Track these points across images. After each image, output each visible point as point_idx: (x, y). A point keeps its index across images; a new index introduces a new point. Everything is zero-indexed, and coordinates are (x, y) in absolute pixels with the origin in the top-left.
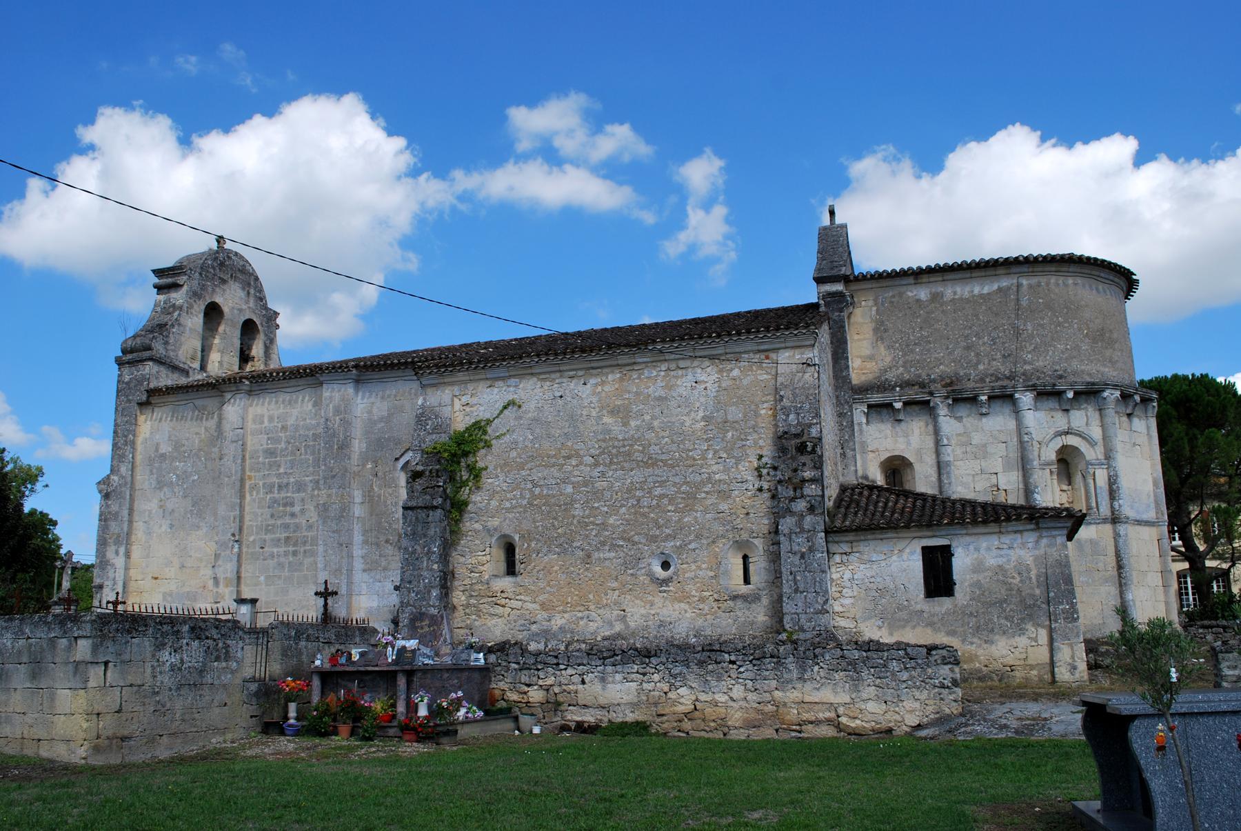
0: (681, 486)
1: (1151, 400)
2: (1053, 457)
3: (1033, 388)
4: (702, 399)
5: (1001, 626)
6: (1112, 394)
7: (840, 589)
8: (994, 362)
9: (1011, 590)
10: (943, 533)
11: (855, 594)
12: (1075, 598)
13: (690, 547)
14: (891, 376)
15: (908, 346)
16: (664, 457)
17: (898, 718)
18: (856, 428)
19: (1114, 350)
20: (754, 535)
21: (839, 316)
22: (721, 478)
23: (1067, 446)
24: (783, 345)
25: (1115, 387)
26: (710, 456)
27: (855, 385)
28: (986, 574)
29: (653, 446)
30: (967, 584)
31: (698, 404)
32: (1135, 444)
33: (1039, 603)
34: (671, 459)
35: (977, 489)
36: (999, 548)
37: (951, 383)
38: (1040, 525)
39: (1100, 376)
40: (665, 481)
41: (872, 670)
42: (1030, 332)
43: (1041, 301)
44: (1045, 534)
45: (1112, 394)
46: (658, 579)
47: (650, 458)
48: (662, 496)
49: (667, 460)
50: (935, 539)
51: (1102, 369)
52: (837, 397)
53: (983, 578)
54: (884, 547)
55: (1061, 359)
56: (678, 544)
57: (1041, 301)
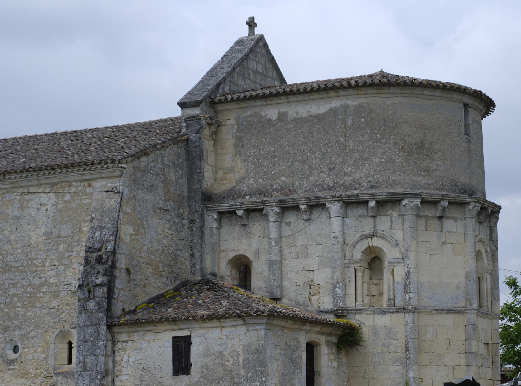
0: (27, 288)
4: (44, 219)
7: (120, 368)
8: (322, 174)
9: (226, 370)
10: (185, 327)
11: (129, 372)
13: (30, 335)
15: (258, 160)
16: (16, 264)
20: (73, 326)
22: (54, 281)
23: (373, 247)
24: (99, 176)
25: (414, 196)
26: (48, 264)
28: (211, 358)
29: (10, 256)
30: (199, 366)
31: (41, 223)
32: (444, 243)
33: (242, 380)
34: (20, 266)
35: (298, 284)
36: (220, 339)
40: (17, 284)
42: (351, 147)
43: (363, 120)
44: (251, 328)
45: (412, 202)
46: (8, 360)
47: (7, 265)
48: (13, 296)
49: (18, 267)
50: (181, 331)
53: (209, 361)
54: (149, 336)
56: (23, 333)
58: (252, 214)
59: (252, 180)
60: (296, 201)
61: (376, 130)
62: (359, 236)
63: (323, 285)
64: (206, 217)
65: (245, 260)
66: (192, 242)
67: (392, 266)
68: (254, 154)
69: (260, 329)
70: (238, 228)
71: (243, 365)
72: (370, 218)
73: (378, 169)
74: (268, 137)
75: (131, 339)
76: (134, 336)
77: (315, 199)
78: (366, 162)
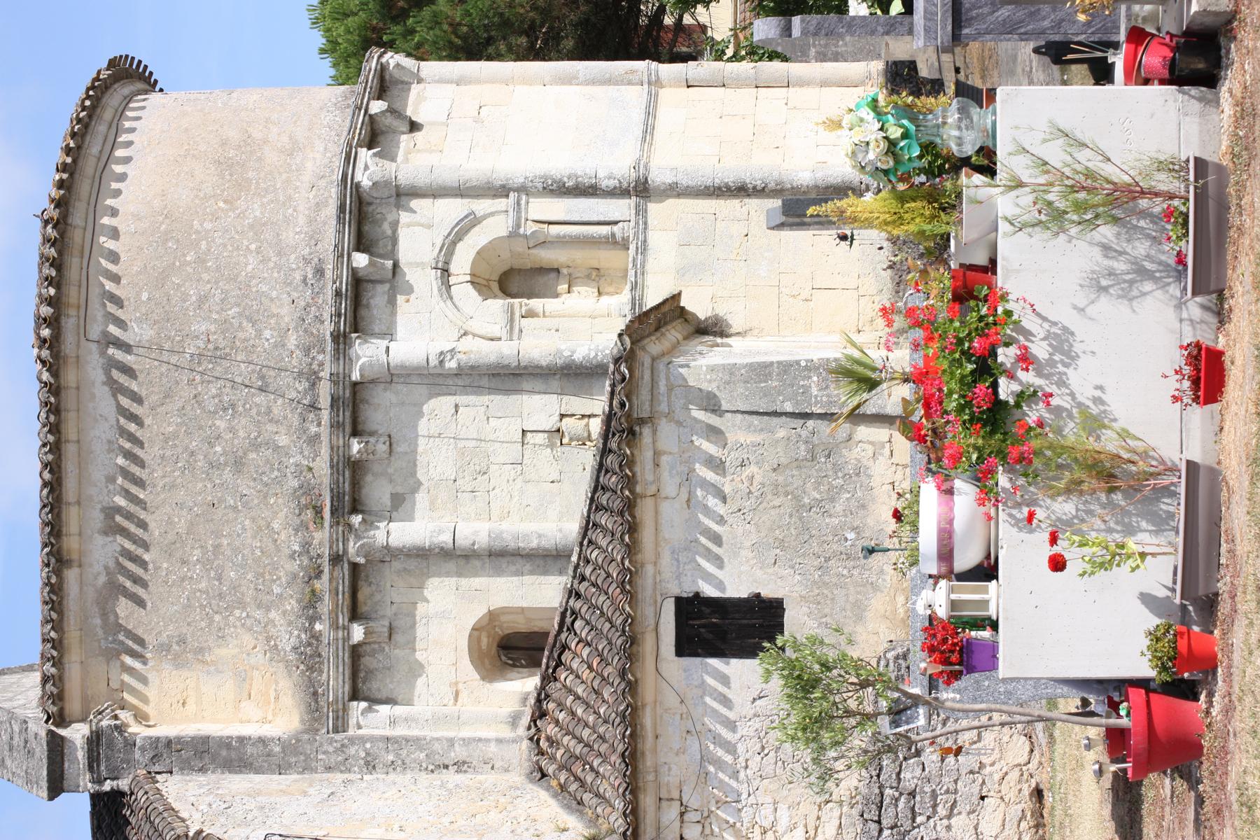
1: (383, 69)
2: (498, 305)
3: (341, 341)
5: (848, 512)
6: (366, 168)
7: (757, 830)
8: (276, 411)
12: (798, 363)
14: (288, 639)
17: (1015, 774)
18: (399, 731)
19: (266, 141)
21: (143, 749)
23: (472, 275)
27: (302, 721)
33: (804, 433)
35: (555, 476)
37: (314, 507)
38: (645, 415)
39: (323, 183)
41: (919, 819)
42: (213, 328)
44: (663, 407)
51: (307, 178)
52: (329, 769)
55: (278, 267)
57: (145, 296)
58: (363, 609)
59: (273, 614)
60: (338, 463)
61: (174, 264)
62: (442, 304)
63: (563, 406)
64: (360, 732)
65: (485, 641)
66: (424, 765)
68: (205, 606)
69: (668, 379)
70: (397, 651)
71: (762, 430)
72: (397, 277)
73: (273, 259)
74: (165, 565)
75: (676, 795)
76: (668, 784)
77: (338, 410)
78: (254, 290)
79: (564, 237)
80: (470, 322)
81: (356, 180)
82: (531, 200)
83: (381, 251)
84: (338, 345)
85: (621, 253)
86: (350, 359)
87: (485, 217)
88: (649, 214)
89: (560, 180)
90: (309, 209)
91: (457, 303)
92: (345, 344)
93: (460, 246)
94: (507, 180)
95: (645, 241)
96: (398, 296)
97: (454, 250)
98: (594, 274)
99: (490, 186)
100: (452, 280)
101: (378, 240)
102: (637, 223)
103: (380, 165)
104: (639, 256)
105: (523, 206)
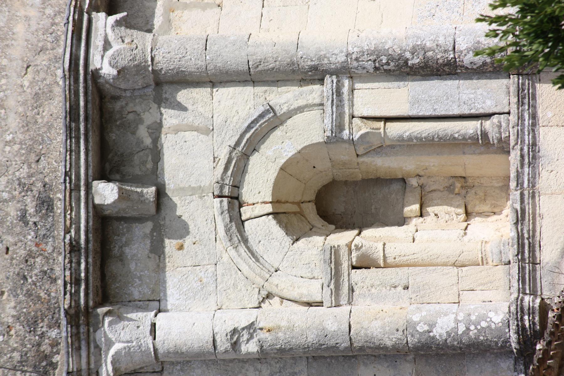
6: (107, 45)
39: (42, 60)
62: (232, 252)
67: (351, 123)
72: (163, 213)
79: (410, 139)
80: (275, 279)
81: (91, 67)
82: (357, 86)
83: (137, 171)
84: (78, 326)
85: (499, 158)
86: (97, 347)
87: (290, 114)
88: (539, 101)
89: (400, 56)
90: (24, 103)
91: (255, 248)
92: (88, 324)
93: (255, 160)
94: (319, 59)
95: (534, 144)
96: (167, 241)
97: (246, 165)
98: (458, 185)
99: (295, 67)
100: (246, 212)
101: (132, 154)
102: (521, 118)
103: (127, 40)
104: (526, 170)
105: (346, 96)
